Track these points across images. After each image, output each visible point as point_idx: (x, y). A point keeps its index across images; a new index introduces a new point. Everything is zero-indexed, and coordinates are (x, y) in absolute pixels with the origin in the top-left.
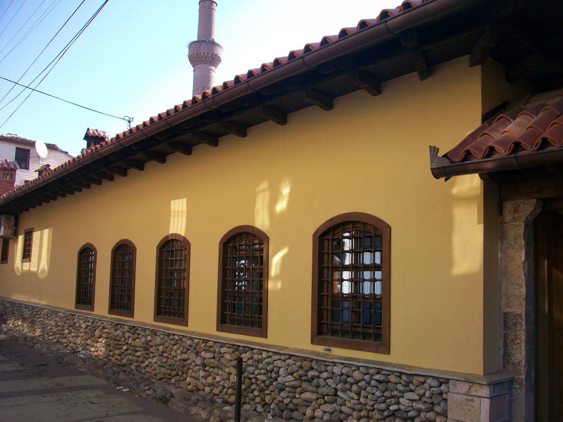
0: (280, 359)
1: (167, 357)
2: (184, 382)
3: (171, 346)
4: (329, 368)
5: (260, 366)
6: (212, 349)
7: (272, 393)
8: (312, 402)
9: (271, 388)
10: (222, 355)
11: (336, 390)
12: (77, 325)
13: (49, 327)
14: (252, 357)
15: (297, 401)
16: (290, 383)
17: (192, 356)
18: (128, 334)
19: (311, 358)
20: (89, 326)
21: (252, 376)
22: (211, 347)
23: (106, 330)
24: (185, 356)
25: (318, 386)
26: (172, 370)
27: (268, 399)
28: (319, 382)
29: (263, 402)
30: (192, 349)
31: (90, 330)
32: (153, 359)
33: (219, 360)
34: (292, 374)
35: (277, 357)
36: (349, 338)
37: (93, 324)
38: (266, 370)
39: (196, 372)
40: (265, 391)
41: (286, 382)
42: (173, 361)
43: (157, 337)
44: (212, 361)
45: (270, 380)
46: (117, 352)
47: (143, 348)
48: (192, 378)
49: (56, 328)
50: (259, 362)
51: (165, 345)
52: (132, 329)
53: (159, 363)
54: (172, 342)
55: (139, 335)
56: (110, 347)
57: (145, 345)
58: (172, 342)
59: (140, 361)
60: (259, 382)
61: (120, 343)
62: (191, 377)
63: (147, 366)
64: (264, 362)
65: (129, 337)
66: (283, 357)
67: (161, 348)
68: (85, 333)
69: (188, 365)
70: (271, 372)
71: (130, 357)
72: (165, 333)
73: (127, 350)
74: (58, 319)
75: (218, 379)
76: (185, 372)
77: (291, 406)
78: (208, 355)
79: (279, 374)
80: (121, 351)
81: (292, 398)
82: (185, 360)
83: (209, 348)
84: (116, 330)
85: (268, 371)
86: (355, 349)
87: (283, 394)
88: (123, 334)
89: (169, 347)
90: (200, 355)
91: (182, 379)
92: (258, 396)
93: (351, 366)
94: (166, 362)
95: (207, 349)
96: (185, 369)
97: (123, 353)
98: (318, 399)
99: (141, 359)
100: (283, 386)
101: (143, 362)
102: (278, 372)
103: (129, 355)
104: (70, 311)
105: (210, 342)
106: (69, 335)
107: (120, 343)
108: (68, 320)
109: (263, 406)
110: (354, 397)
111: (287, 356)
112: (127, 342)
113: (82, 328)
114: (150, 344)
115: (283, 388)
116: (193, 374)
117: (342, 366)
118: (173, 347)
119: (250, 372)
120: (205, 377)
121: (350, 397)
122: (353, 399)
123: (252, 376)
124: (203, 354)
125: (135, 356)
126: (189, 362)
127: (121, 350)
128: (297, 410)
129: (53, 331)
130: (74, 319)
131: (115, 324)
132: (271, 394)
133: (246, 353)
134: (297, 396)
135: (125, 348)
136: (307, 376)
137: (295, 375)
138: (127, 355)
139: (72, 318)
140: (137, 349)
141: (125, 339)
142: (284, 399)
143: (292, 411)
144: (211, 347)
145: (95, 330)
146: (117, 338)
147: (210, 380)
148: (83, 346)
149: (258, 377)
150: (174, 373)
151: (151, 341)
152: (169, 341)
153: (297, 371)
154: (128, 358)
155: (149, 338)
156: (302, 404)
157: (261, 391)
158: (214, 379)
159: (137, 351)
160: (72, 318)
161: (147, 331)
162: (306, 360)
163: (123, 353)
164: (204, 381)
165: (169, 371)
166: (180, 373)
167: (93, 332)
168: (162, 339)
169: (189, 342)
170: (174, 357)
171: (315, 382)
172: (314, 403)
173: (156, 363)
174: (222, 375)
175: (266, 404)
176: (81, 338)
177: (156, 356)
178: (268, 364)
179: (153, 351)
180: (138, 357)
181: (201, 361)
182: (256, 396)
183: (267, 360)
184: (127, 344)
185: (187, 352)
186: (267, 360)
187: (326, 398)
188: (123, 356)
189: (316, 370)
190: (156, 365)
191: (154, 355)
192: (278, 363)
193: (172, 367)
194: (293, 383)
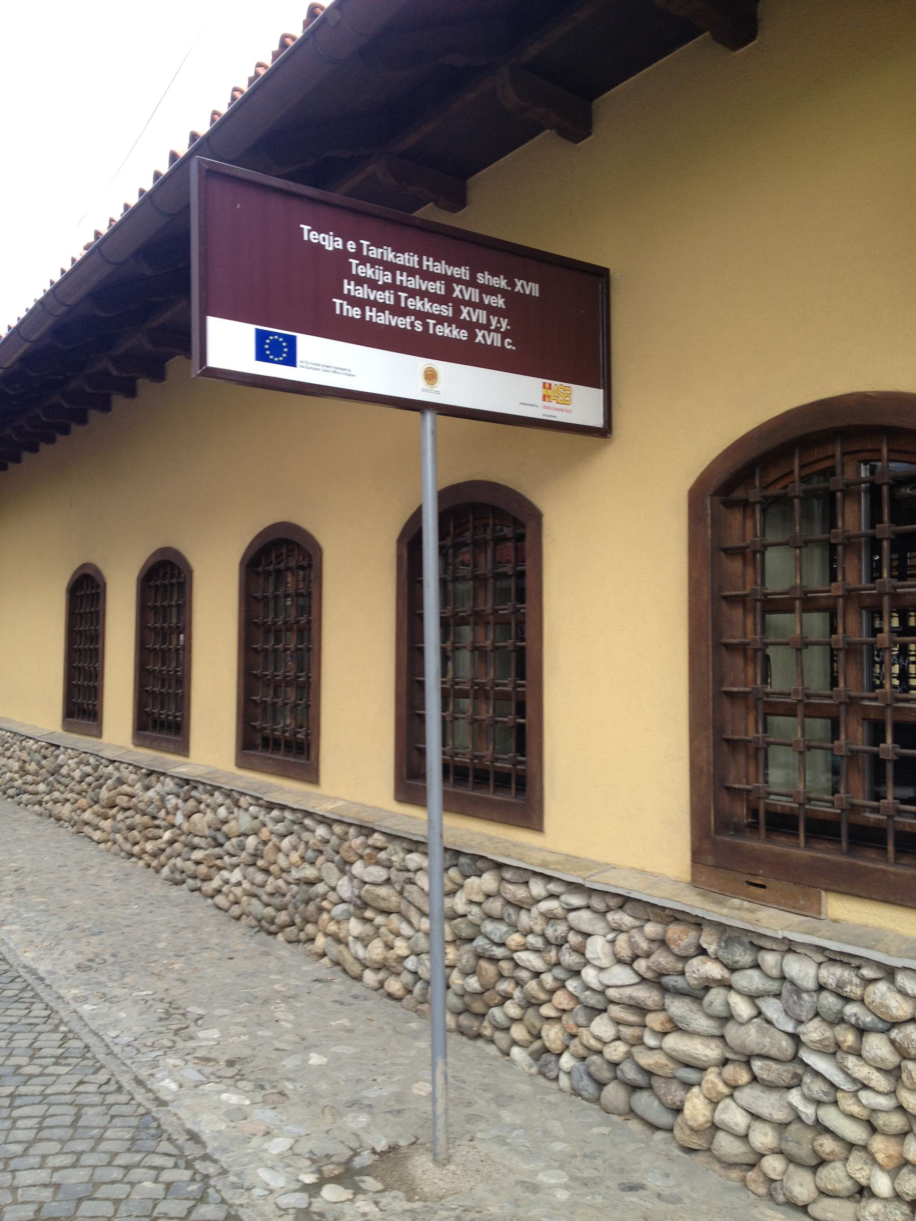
0: (588, 907)
1: (266, 871)
2: (309, 946)
3: (275, 839)
4: (769, 960)
5: (524, 919)
6: (382, 855)
7: (565, 1017)
8: (703, 1069)
9: (561, 999)
10: (409, 876)
11: (795, 1038)
12: (64, 771)
13: (8, 775)
14: (604, 1085)
15: (651, 1062)
16: (621, 990)
17: (330, 872)
18: (172, 801)
19: (697, 916)
20: (89, 775)
21: (499, 952)
22: (381, 849)
23: (125, 788)
24: (309, 872)
25: (727, 1018)
26: (279, 909)
27: (553, 1035)
28: (728, 1004)
29: (537, 1045)
30: (328, 849)
31: (89, 785)
32: (232, 872)
33: (401, 893)
34: (629, 963)
35: (576, 900)
36: (798, 846)
37: (96, 768)
38: (543, 935)
39: (338, 922)
40: (540, 1005)
41: (609, 987)
42: (280, 882)
43: (242, 813)
44: (383, 891)
45: (559, 973)
46: (150, 846)
47: (209, 839)
48: (329, 939)
49: (21, 777)
50: (521, 908)
51: (260, 834)
52: (182, 787)
53: (246, 885)
54: (280, 828)
55: (200, 803)
56: (135, 833)
57: (212, 833)
58: (280, 828)
59: (202, 877)
60: (524, 975)
61: (157, 822)
62: (327, 935)
63: (219, 891)
64: (534, 910)
65: (177, 808)
66: (598, 904)
67: (251, 842)
68: (79, 794)
69: (318, 900)
70: (559, 946)
71: (178, 862)
72: (261, 802)
73: (172, 842)
74: (24, 756)
75: (401, 948)
76: (312, 919)
77: (629, 1072)
78: (377, 873)
79: (583, 954)
80: (160, 844)
81: (633, 1045)
82: (311, 883)
83: (374, 852)
84: (147, 788)
85: (548, 942)
86: (886, 901)
87: (602, 1027)
88: (162, 799)
89: (270, 840)
90: (350, 871)
91: (302, 936)
92: (520, 1020)
93: (855, 962)
94: (262, 886)
95: (369, 855)
96: (312, 907)
97: (163, 850)
98: (725, 1062)
99: (203, 869)
100: (600, 997)
101: (207, 879)
102: (580, 951)
103: (176, 857)
104: (122, 747)
105: (376, 836)
106: (47, 798)
107: (157, 822)
108: (45, 758)
109: (536, 1056)
110: (873, 1084)
111: (613, 902)
112: (172, 822)
113: (73, 779)
114: (225, 828)
115: (600, 1007)
116: (332, 928)
117: (820, 959)
118: (281, 840)
119: (492, 937)
120: (364, 941)
121: (855, 1080)
122: (865, 1087)
123: (499, 952)
124: (358, 868)
125: (189, 860)
126: (321, 888)
127: (159, 841)
128: (650, 1087)
129: (16, 784)
130: (57, 757)
131: (144, 771)
132: (559, 1019)
133: (480, 876)
134: (650, 1041)
135: (167, 835)
136: (682, 973)
137: (641, 965)
138: (169, 858)
139: (53, 752)
140: (196, 841)
141: (168, 813)
142: (605, 1043)
143: (634, 1088)
144: (381, 849)
145: (100, 787)
146: (149, 810)
147: (376, 950)
148: (75, 828)
149: (516, 956)
150: (283, 917)
151: (225, 822)
152: (270, 825)
153: (648, 955)
154: (175, 865)
155: (222, 812)
156: (667, 1072)
157: (531, 1003)
158: (389, 947)
159: (194, 848)
160: (53, 752)
161: (217, 794)
162: (676, 919)
163: (163, 850)
164: (361, 952)
165: (270, 911)
166: (298, 920)
167: (97, 790)
168: (256, 818)
169: (321, 831)
170: (283, 870)
171: (716, 997)
172: (711, 1076)
173: (239, 884)
174: (409, 938)
175: (547, 1051)
176: (73, 804)
177: (237, 865)
178: (550, 918)
179: (232, 851)
180: (198, 863)
181: (353, 892)
182: (514, 1020)
183: (545, 906)
184: (173, 826)
185: (316, 858)
186: (545, 906)
187: (757, 1065)
188: (163, 858)
189: (717, 959)
190: (238, 891)
191: (234, 860)
192: (582, 919)
193: (277, 901)
194: (634, 994)
